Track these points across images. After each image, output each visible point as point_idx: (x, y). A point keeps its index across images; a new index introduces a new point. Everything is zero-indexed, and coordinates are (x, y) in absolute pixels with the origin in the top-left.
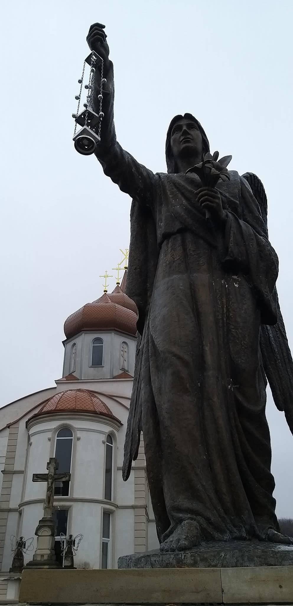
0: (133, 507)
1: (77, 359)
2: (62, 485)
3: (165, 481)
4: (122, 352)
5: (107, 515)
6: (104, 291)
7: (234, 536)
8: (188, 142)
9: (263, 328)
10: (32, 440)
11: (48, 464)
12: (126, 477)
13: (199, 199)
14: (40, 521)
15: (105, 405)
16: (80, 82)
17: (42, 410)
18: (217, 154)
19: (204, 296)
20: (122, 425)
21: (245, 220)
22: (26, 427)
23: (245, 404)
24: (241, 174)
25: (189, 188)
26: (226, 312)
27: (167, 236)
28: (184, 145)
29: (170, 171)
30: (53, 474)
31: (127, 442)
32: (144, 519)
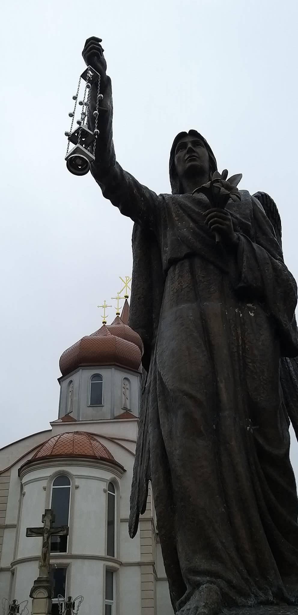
0: (139, 564)
1: (74, 398)
2: (59, 540)
3: (179, 539)
4: (124, 390)
5: (110, 573)
6: (103, 323)
7: (259, 601)
8: (194, 160)
9: (282, 361)
10: (26, 489)
11: (44, 516)
12: (133, 533)
13: (209, 220)
14: (35, 581)
15: (105, 449)
16: (75, 98)
17: (37, 455)
18: (226, 172)
19: (216, 327)
20: (125, 471)
21: (258, 243)
22: (19, 476)
23: (267, 448)
24: (252, 193)
25: (197, 210)
26: (242, 344)
27: (173, 262)
28: (190, 164)
29: (175, 191)
30: (49, 528)
31: (133, 494)
32: (151, 577)
